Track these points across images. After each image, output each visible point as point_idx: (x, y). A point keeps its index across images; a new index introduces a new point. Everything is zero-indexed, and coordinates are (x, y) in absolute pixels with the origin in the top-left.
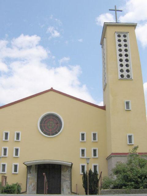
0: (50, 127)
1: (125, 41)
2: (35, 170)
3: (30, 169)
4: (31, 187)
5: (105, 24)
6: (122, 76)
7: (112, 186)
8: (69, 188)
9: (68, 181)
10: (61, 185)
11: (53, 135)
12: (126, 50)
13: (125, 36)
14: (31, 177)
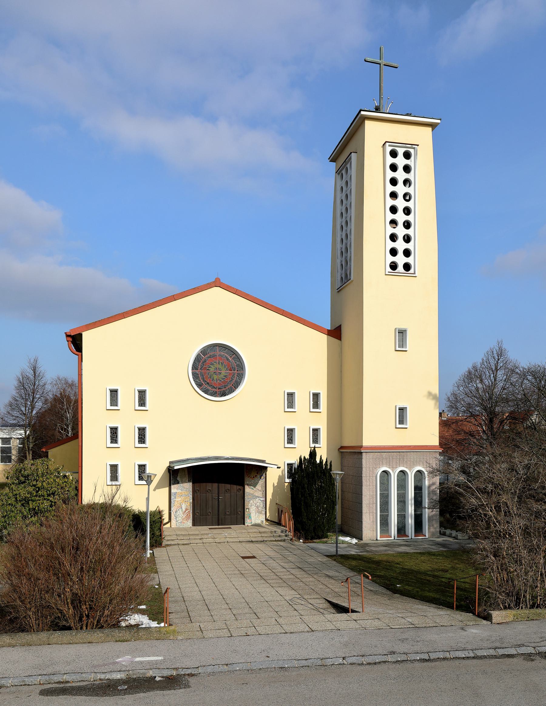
0: (215, 377)
1: (407, 169)
2: (187, 475)
3: (177, 476)
4: (180, 513)
5: (362, 113)
6: (394, 266)
7: (440, 418)
8: (261, 513)
9: (259, 497)
10: (246, 507)
11: (221, 396)
12: (407, 211)
13: (407, 155)
14: (179, 491)
